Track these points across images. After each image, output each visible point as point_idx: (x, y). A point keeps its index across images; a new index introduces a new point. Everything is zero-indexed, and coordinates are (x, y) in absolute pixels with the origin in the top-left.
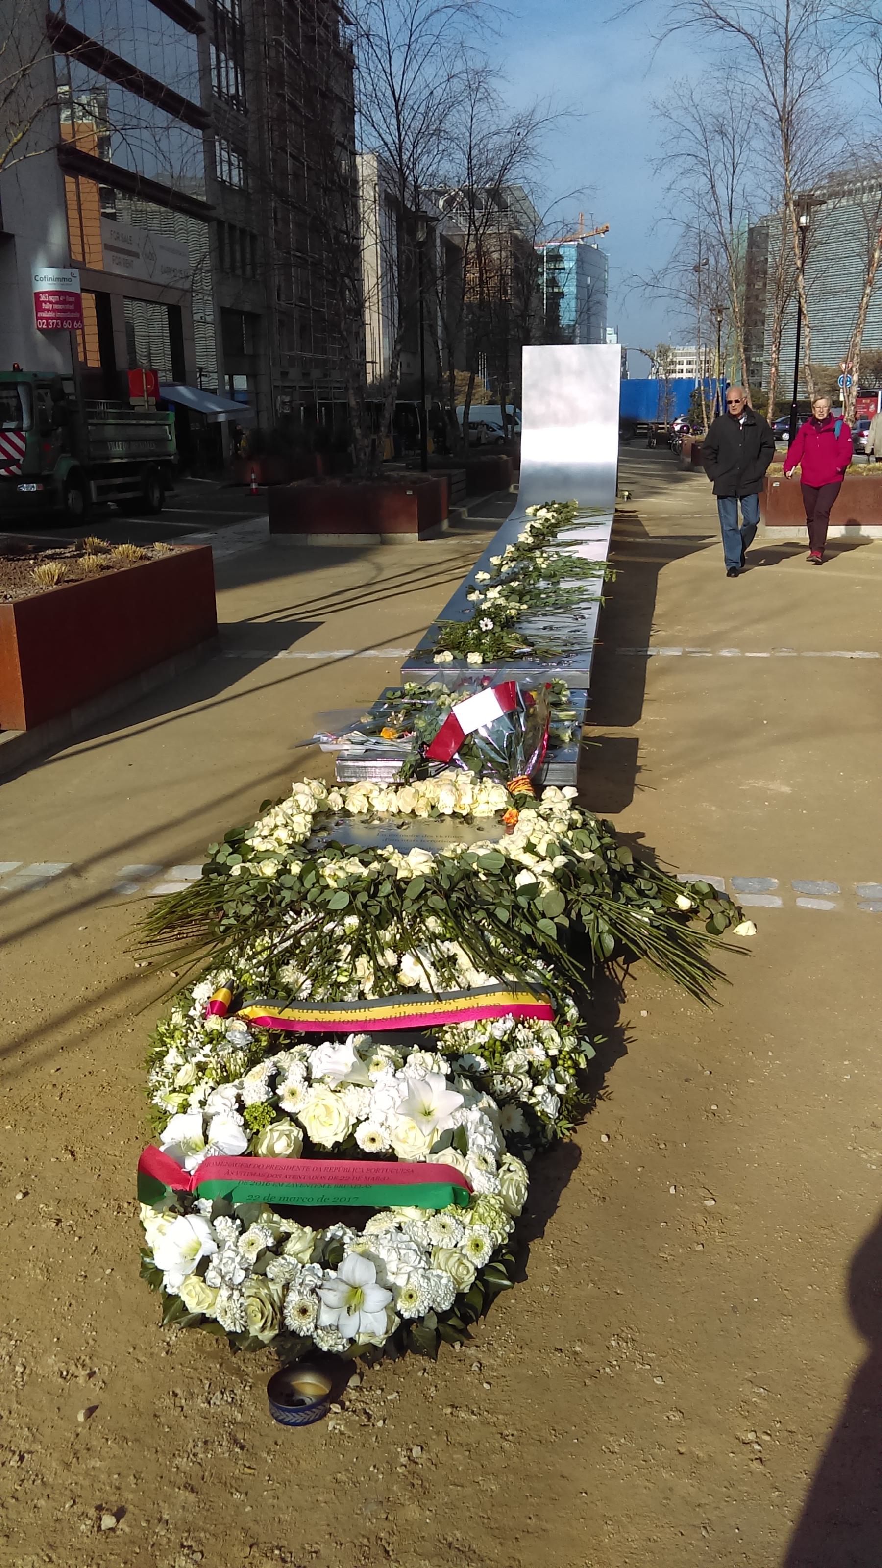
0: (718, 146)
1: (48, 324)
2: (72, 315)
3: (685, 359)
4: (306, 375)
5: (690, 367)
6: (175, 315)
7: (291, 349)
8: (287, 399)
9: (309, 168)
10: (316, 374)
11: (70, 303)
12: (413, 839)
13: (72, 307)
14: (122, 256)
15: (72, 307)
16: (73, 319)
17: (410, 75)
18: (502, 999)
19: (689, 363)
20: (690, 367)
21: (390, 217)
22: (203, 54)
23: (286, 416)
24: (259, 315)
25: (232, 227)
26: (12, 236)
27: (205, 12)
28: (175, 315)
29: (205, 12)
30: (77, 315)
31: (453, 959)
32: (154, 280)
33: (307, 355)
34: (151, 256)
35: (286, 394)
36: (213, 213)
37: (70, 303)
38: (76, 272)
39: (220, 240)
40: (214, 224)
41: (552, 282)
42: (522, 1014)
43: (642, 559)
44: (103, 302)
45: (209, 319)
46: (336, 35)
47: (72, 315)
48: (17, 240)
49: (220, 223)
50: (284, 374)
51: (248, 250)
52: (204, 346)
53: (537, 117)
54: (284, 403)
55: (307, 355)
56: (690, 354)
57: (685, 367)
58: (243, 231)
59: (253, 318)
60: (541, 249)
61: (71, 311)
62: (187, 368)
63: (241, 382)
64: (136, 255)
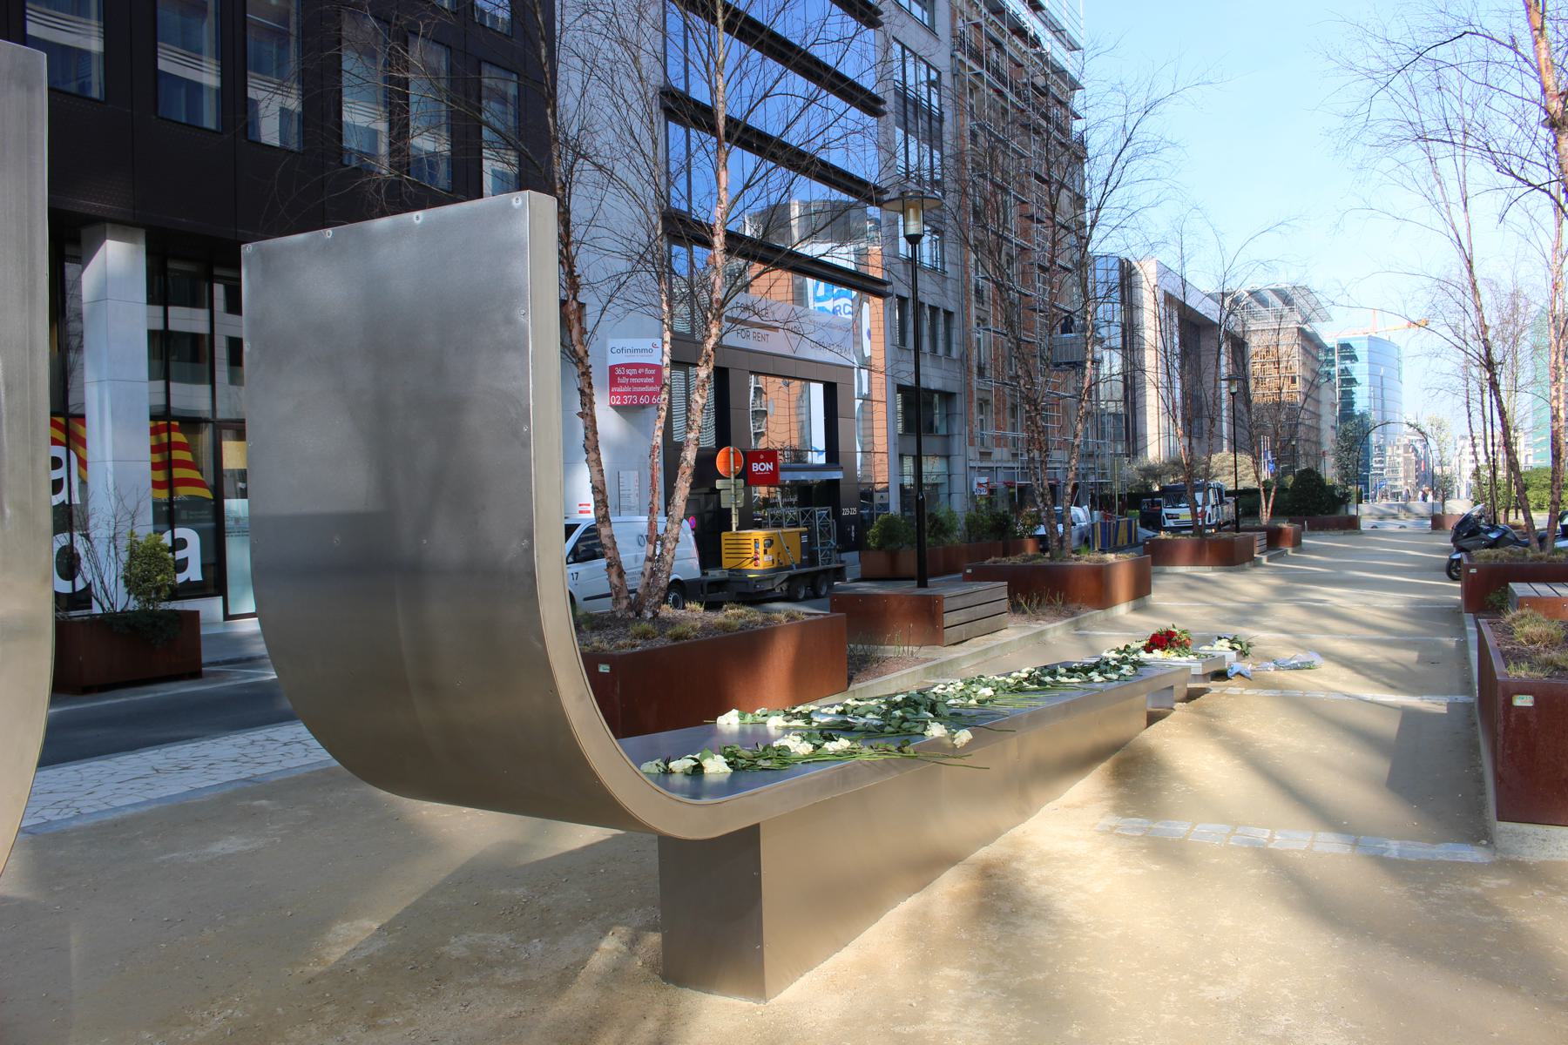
6: (830, 391)
8: (984, 480)
13: (651, 380)
15: (651, 380)
16: (651, 394)
35: (982, 475)
47: (651, 389)
50: (985, 455)
54: (980, 485)
59: (947, 396)
61: (650, 385)
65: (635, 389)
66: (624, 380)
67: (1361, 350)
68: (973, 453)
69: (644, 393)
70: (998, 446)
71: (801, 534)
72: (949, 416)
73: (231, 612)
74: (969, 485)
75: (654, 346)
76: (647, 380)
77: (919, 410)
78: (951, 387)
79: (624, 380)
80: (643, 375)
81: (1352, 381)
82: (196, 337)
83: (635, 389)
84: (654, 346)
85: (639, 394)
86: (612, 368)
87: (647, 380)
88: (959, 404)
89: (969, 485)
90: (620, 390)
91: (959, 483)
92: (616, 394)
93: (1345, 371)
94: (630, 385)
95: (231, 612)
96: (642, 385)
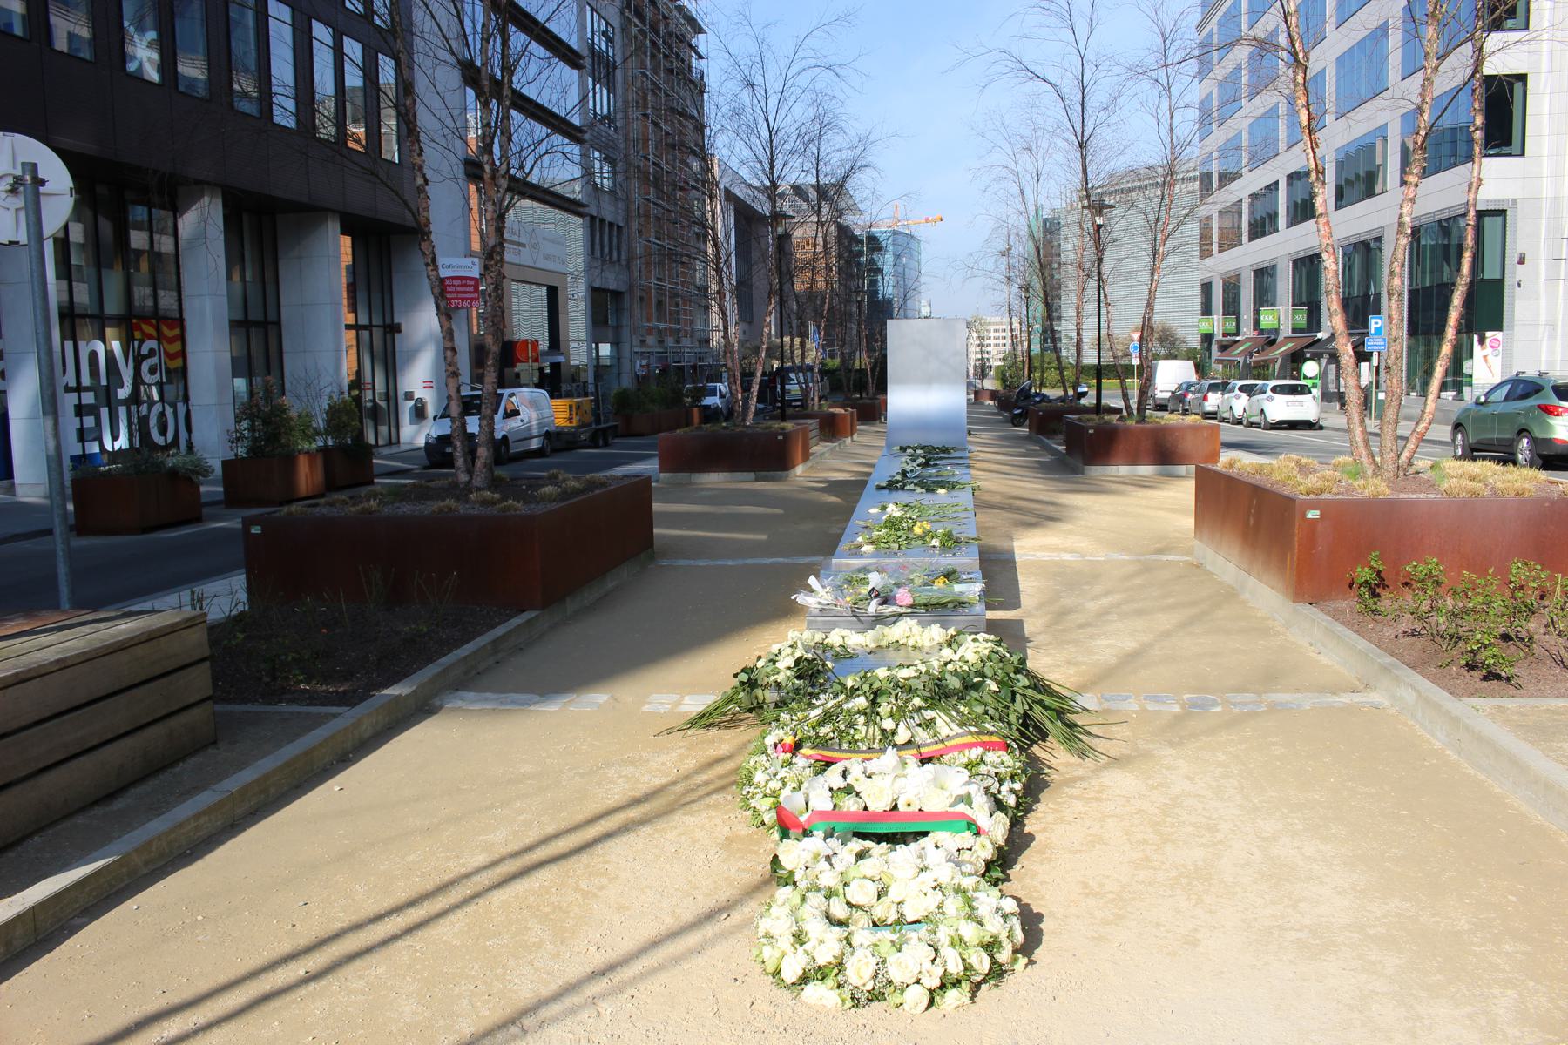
0: (1025, 160)
3: (992, 328)
4: (661, 342)
6: (553, 292)
7: (649, 320)
8: (644, 362)
10: (670, 341)
17: (782, 114)
18: (970, 739)
21: (901, 276)
22: (583, 84)
25: (602, 221)
27: (585, 52)
29: (585, 52)
31: (933, 720)
32: (538, 265)
33: (662, 325)
34: (535, 246)
36: (586, 210)
41: (486, 105)
42: (988, 747)
43: (768, 561)
46: (690, 67)
49: (593, 218)
50: (643, 342)
53: (872, 138)
55: (662, 325)
58: (611, 224)
59: (617, 295)
63: (605, 349)
64: (523, 245)
68: (636, 342)
72: (619, 311)
77: (606, 308)
78: (622, 288)
88: (627, 298)
93: (872, 262)
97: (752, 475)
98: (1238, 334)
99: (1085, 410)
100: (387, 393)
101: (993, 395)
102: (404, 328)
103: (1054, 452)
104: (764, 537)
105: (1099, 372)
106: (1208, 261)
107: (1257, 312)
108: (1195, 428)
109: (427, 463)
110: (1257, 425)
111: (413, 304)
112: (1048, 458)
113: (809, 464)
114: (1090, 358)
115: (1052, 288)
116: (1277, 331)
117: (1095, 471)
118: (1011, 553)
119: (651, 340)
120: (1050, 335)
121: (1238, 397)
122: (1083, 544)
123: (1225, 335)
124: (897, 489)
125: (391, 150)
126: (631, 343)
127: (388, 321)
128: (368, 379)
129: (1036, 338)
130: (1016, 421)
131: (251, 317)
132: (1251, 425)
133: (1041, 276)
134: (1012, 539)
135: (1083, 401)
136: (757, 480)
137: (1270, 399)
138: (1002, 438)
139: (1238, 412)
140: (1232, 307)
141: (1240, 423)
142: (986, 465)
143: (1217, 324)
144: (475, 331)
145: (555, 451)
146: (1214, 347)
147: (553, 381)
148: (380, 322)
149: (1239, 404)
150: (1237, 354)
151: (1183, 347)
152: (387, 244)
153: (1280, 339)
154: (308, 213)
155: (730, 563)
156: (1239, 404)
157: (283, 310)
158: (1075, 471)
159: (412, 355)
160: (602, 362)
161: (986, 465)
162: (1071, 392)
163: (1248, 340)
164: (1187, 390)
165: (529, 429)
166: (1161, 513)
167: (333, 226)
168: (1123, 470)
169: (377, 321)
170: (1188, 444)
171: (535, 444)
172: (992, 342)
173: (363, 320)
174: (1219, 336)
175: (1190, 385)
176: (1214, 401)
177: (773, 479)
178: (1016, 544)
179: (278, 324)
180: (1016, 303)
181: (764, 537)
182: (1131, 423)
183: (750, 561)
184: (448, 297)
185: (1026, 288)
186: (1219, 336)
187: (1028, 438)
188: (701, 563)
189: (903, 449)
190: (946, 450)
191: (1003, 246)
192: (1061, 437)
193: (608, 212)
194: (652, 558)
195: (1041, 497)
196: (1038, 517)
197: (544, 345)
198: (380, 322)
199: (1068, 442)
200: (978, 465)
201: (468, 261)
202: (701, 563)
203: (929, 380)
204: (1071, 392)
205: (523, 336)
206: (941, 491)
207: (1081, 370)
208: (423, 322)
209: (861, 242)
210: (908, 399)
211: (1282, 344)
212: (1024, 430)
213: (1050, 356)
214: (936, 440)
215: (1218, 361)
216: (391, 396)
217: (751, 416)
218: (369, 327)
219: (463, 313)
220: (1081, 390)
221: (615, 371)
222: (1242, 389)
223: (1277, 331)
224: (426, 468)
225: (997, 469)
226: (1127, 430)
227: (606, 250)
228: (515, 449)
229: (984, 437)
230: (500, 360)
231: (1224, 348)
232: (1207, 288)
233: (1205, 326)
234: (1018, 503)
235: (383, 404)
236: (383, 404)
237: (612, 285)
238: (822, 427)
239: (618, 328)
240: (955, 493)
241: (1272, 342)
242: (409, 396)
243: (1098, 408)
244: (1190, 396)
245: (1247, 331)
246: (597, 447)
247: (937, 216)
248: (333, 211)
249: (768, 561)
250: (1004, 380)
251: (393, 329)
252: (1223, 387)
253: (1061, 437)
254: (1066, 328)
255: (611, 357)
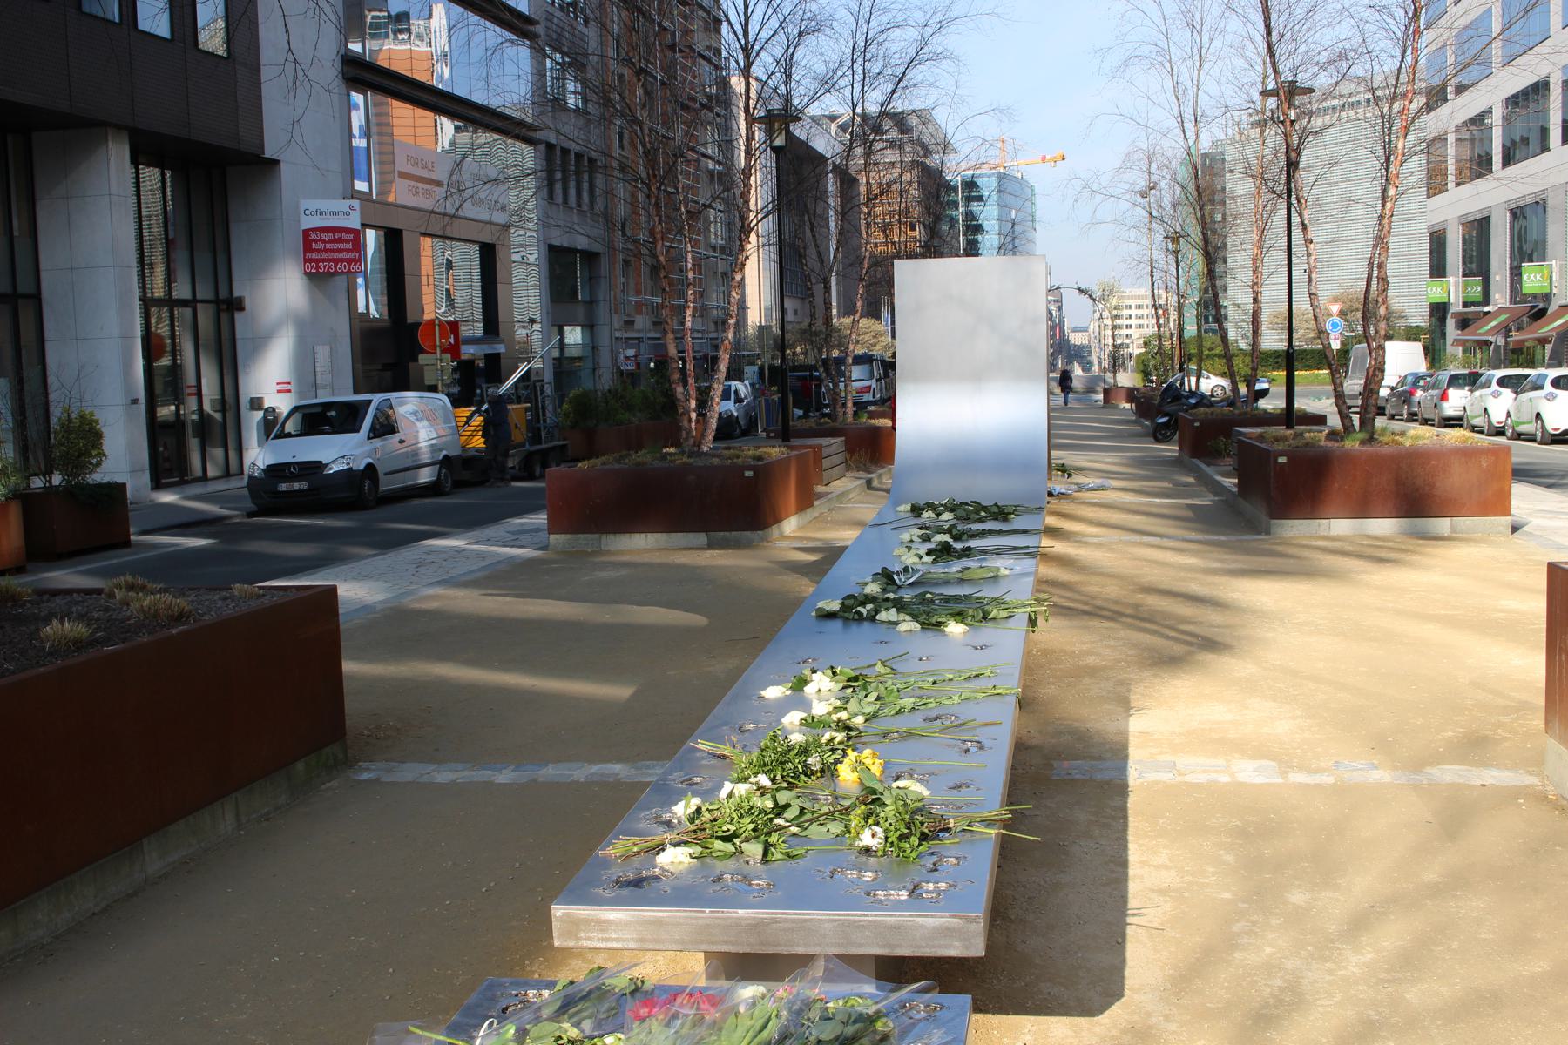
1: (318, 267)
2: (349, 256)
3: (1134, 303)
5: (1140, 312)
6: (488, 254)
7: (638, 292)
8: (631, 352)
9: (663, 84)
11: (347, 241)
12: (1318, 122)
13: (349, 246)
14: (421, 185)
15: (349, 246)
16: (349, 261)
19: (1139, 307)
20: (1140, 312)
23: (631, 374)
24: (598, 254)
26: (276, 162)
28: (488, 254)
30: (355, 255)
35: (628, 347)
36: (540, 135)
37: (347, 241)
38: (356, 203)
39: (550, 171)
40: (542, 147)
43: (580, 772)
44: (393, 241)
45: (532, 259)
47: (349, 256)
48: (284, 168)
49: (550, 147)
50: (629, 324)
51: (585, 186)
52: (526, 290)
54: (627, 358)
56: (1139, 297)
57: (1134, 312)
58: (579, 156)
59: (590, 257)
60: (953, 175)
61: (348, 251)
62: (501, 318)
63: (574, 335)
65: (332, 256)
66: (320, 246)
67: (988, 186)
68: (617, 321)
69: (342, 260)
70: (640, 313)
71: (527, 409)
72: (592, 280)
73: (1480, 299)
74: (614, 359)
75: (351, 207)
76: (344, 246)
77: (567, 273)
78: (597, 248)
79: (320, 246)
80: (340, 241)
81: (978, 229)
82: (1319, 351)
83: (332, 256)
84: (351, 207)
85: (336, 261)
86: (306, 232)
87: (344, 246)
88: (604, 261)
89: (614, 359)
90: (314, 256)
91: (605, 359)
92: (310, 260)
93: (970, 215)
94: (326, 251)
95: (1480, 299)
96: (340, 251)
97: (702, 538)
98: (1486, 301)
99: (1267, 419)
100: (223, 401)
101: (1131, 394)
102: (247, 303)
103: (1217, 488)
104: (620, 692)
105: (1290, 360)
106: (1439, 199)
107: (1516, 273)
108: (1467, 453)
109: (250, 505)
110: (1531, 438)
111: (262, 267)
112: (1205, 501)
113: (810, 514)
114: (1273, 341)
115: (1217, 249)
116: (1547, 297)
117: (1295, 529)
118: (1118, 753)
119: (641, 321)
120: (1212, 308)
121: (1496, 395)
122: (1283, 725)
123: (1465, 305)
124: (860, 618)
125: (212, 37)
126: (610, 325)
127: (223, 294)
128: (190, 378)
129: (1190, 315)
130: (1160, 434)
131: (199, 296)
132: (1519, 436)
133: (1200, 215)
134: (1125, 705)
135: (1264, 404)
136: (711, 546)
137: (1550, 398)
138: (1140, 463)
139: (1498, 417)
140: (1477, 264)
141: (1500, 432)
142: (1104, 515)
143: (1454, 289)
144: (361, 308)
145: (459, 485)
146: (1451, 323)
147: (470, 383)
148: (210, 295)
149: (1500, 405)
150: (1485, 330)
151: (1401, 324)
152: (213, 177)
153: (1552, 308)
154: (78, 129)
155: (505, 776)
156: (1500, 405)
157: (43, 275)
158: (1255, 527)
159: (261, 342)
160: (569, 353)
161: (1104, 515)
162: (1243, 390)
163: (1501, 310)
164: (1415, 384)
165: (416, 453)
166: (1430, 631)
167: (116, 157)
168: (1341, 527)
169: (204, 292)
170: (1456, 479)
171: (425, 476)
172: (1134, 322)
173: (182, 291)
174: (1456, 307)
175: (1418, 377)
176: (1457, 401)
177: (737, 545)
178: (1136, 725)
179: (37, 297)
180: (1158, 255)
181: (620, 692)
182: (1352, 444)
183: (551, 772)
184: (326, 256)
185: (1175, 238)
186: (1456, 307)
187: (1176, 462)
188: (444, 776)
189: (916, 510)
190: (1001, 513)
191: (1142, 184)
192: (1228, 463)
193: (571, 134)
194: (347, 762)
195: (1195, 588)
196: (1182, 639)
197: (474, 328)
198: (210, 295)
199: (1241, 472)
200: (1089, 512)
201: (344, 205)
202: (444, 776)
203: (976, 375)
204: (1243, 390)
205: (427, 317)
206: (955, 629)
207: (1260, 359)
208: (281, 292)
209: (955, 189)
210: (928, 416)
211: (1557, 315)
212: (1172, 449)
213: (1211, 340)
214: (987, 490)
215: (1457, 342)
216: (230, 403)
217: (710, 436)
218: (191, 303)
219: (341, 281)
220: (1259, 386)
221: (589, 365)
222: (1503, 382)
223: (1547, 297)
224: (251, 515)
225: (1123, 531)
226: (1348, 457)
227: (585, 196)
228: (386, 485)
229: (1108, 461)
230: (391, 350)
231: (1464, 323)
232: (1438, 242)
233: (1436, 292)
234: (1153, 601)
235: (218, 416)
236: (218, 416)
237: (582, 243)
238: (851, 449)
239: (591, 303)
240: (988, 633)
241: (1539, 315)
242: (256, 404)
243: (1290, 417)
244: (1419, 394)
245: (1501, 297)
246: (531, 478)
247: (1058, 154)
248: (119, 127)
249: (580, 772)
250: (1146, 374)
251: (230, 306)
252: (1472, 381)
253: (1228, 463)
254: (1236, 297)
255: (583, 346)
